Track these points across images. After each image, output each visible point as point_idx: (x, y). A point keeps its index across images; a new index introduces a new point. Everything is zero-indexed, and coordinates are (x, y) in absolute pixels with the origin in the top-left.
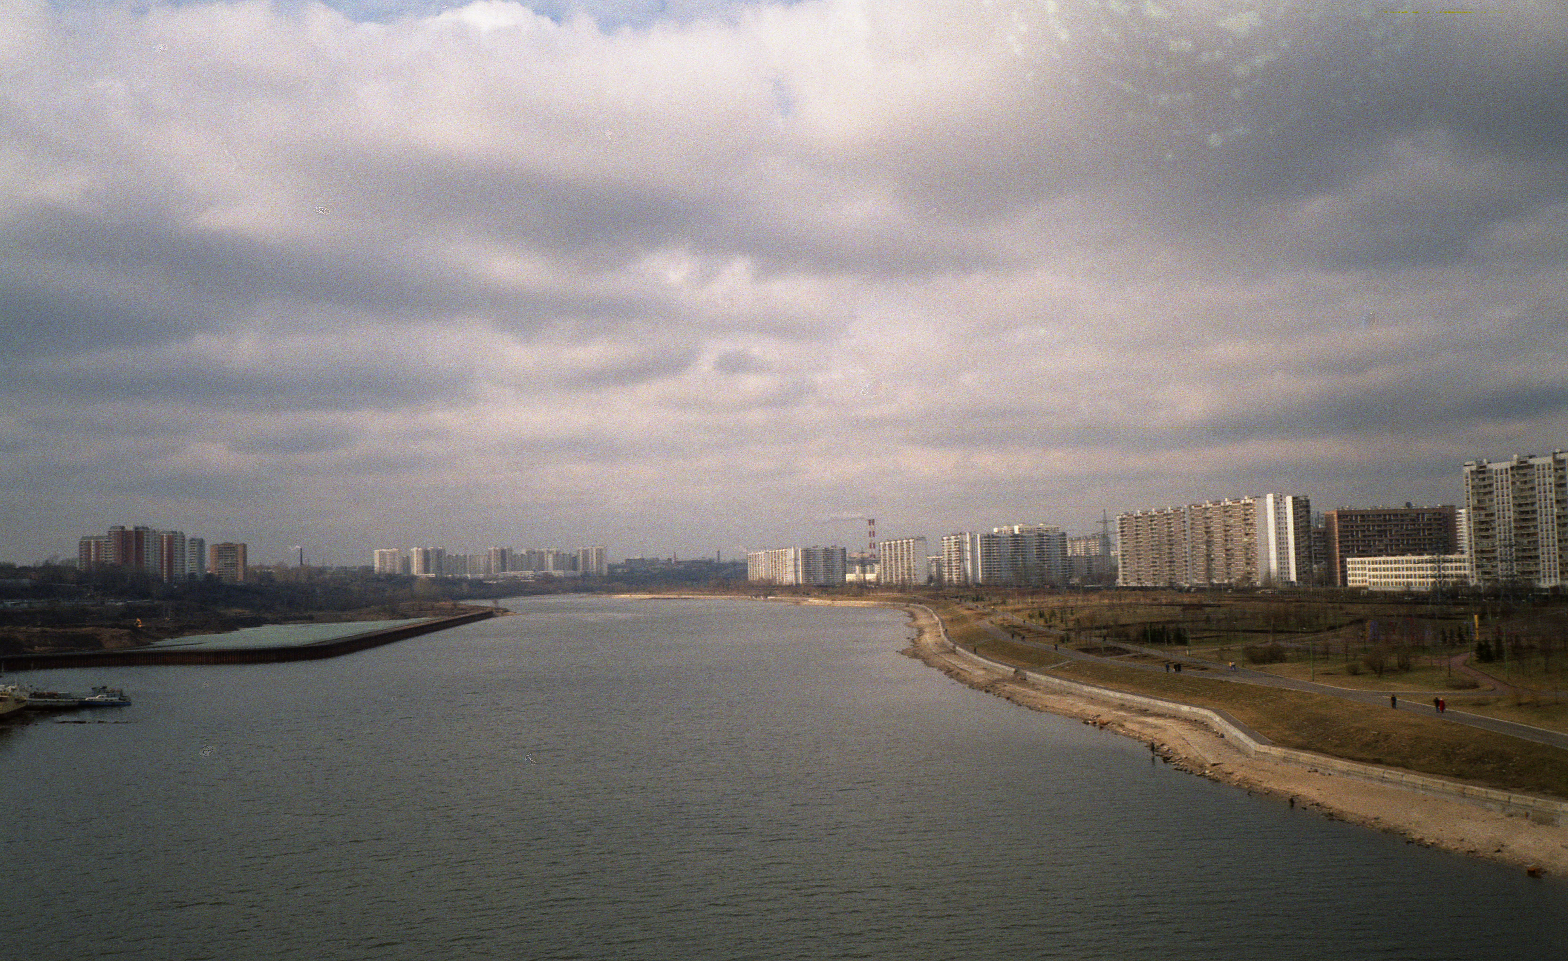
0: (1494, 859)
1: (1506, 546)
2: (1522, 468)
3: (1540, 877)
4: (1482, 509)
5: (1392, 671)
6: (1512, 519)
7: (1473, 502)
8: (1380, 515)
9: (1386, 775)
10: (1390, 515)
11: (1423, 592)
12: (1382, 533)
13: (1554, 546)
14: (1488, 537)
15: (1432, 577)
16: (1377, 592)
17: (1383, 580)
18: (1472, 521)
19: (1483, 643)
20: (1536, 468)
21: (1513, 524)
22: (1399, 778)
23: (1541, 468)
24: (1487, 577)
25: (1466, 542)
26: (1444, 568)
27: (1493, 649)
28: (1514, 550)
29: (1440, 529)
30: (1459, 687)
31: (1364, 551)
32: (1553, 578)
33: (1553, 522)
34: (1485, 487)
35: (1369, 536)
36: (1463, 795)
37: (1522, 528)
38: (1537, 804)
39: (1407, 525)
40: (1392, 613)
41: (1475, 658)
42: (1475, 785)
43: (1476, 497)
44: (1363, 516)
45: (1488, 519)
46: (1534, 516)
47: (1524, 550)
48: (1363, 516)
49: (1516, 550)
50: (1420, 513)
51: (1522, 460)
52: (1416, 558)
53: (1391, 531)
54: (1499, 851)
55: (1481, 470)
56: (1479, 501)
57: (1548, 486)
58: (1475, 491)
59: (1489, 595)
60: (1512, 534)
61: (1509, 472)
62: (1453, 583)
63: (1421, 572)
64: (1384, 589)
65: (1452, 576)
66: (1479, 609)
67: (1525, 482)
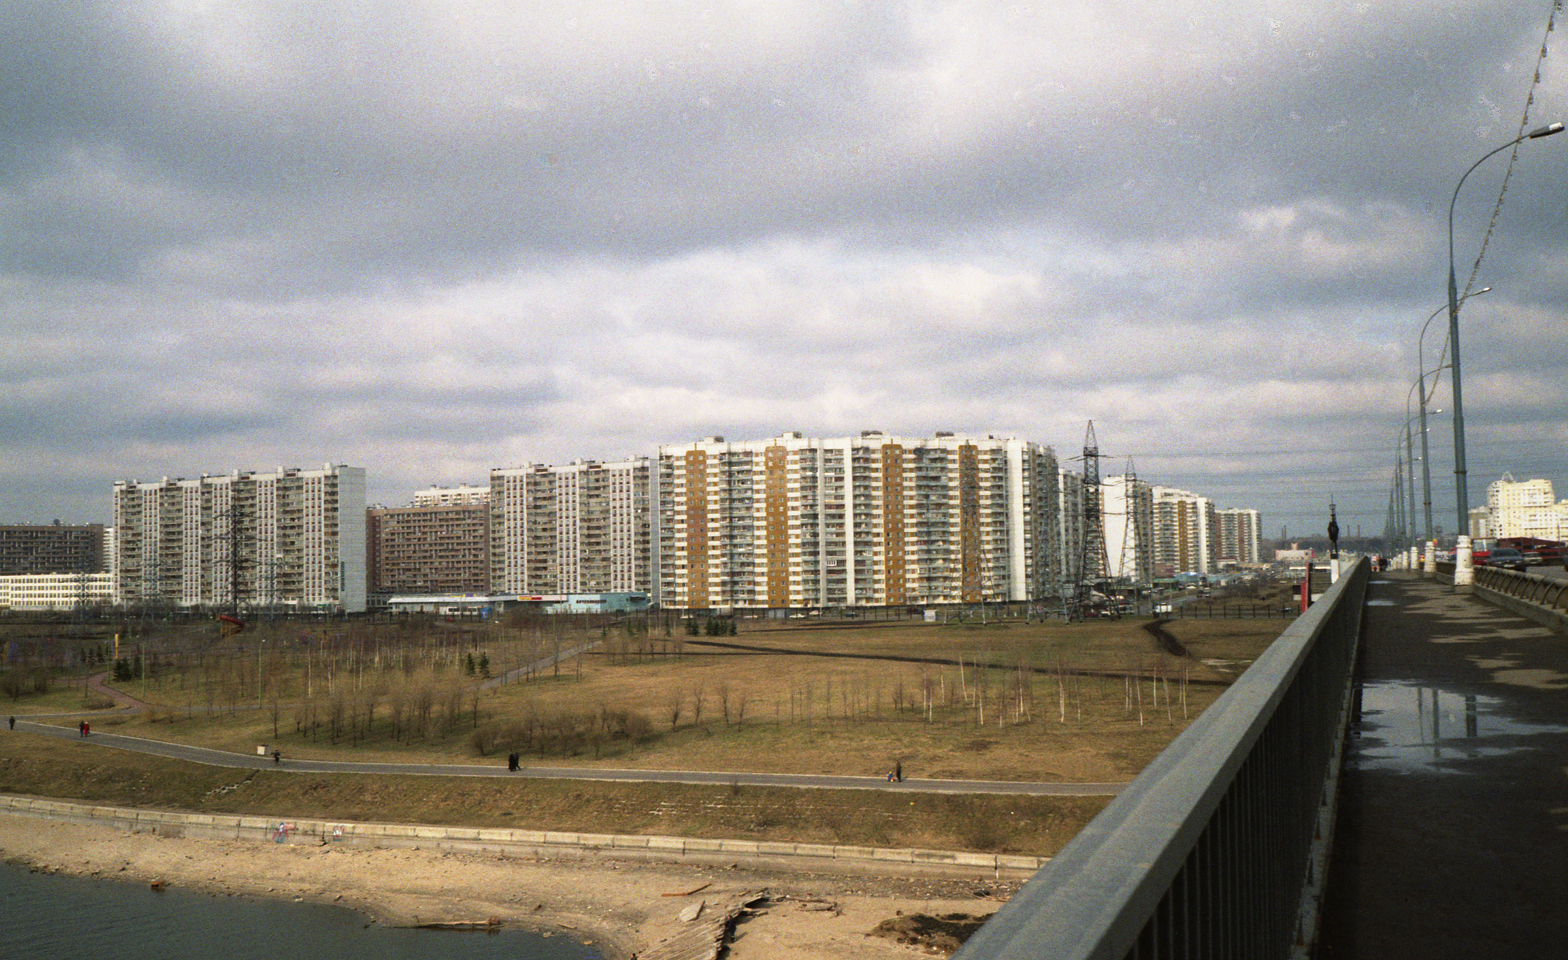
0: (117, 877)
1: (151, 566)
2: (171, 490)
3: (163, 890)
4: (131, 528)
5: (28, 694)
6: (158, 539)
7: (121, 522)
8: (27, 532)
9: (14, 803)
10: (37, 532)
11: (65, 612)
12: (28, 550)
13: (197, 566)
14: (133, 557)
15: (76, 596)
16: (19, 612)
17: (26, 599)
18: (119, 541)
19: (122, 662)
20: (184, 490)
21: (159, 545)
22: (27, 805)
23: (189, 491)
24: (130, 596)
25: (113, 561)
26: (88, 588)
27: (131, 668)
28: (158, 569)
29: (87, 548)
30: (93, 707)
31: (7, 569)
32: (194, 597)
33: (197, 543)
34: (134, 506)
35: (15, 553)
36: (92, 816)
37: (167, 548)
38: (163, 819)
39: (54, 542)
40: (32, 633)
41: (113, 678)
42: (104, 805)
43: (124, 517)
44: (8, 532)
45: (134, 539)
46: (180, 537)
47: (168, 570)
48: (8, 532)
49: (160, 570)
50: (69, 531)
51: (244, 476)
52: (61, 576)
53: (37, 548)
54: (124, 869)
55: (131, 490)
56: (127, 521)
57: (194, 509)
58: (124, 510)
59: (132, 614)
60: (158, 555)
61: (275, 485)
62: (96, 602)
63: (65, 592)
64: (26, 608)
65: (96, 595)
66: (120, 627)
67: (173, 504)
